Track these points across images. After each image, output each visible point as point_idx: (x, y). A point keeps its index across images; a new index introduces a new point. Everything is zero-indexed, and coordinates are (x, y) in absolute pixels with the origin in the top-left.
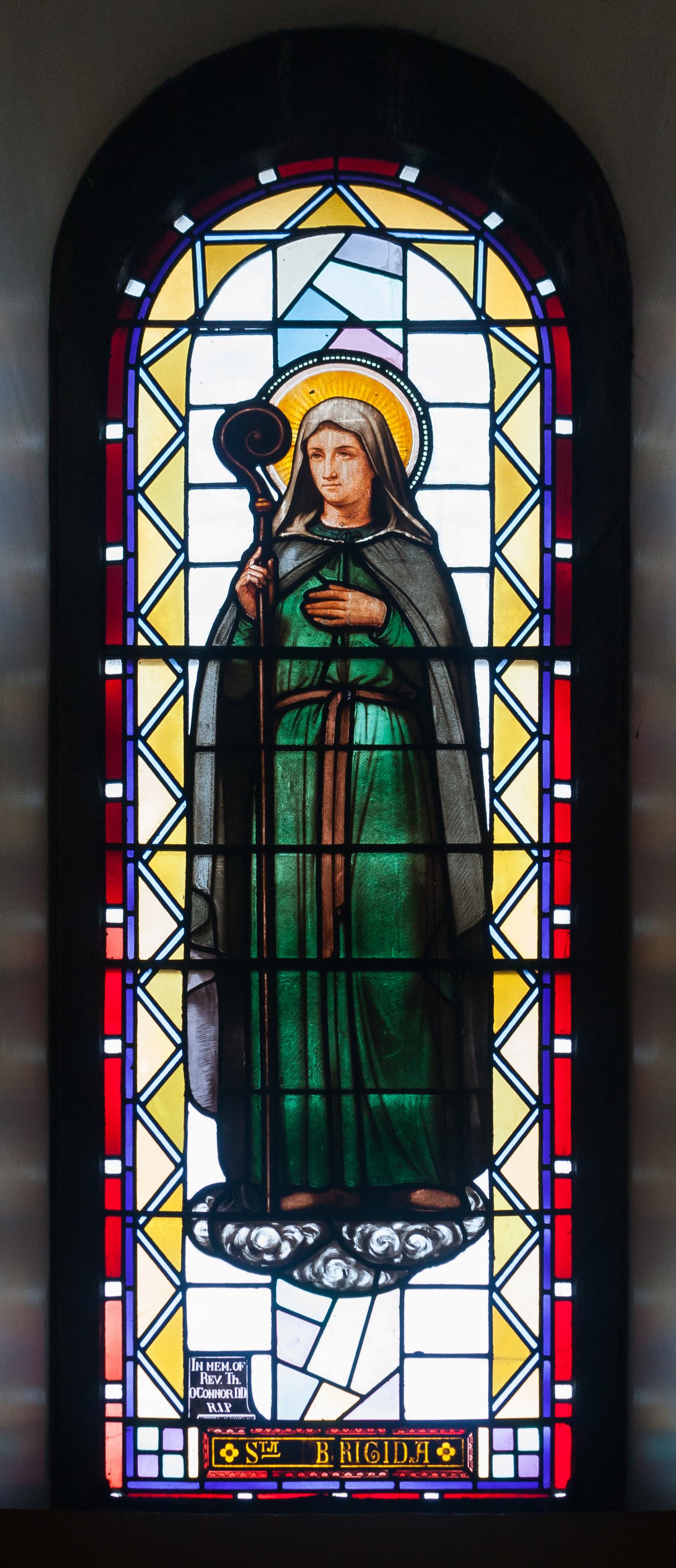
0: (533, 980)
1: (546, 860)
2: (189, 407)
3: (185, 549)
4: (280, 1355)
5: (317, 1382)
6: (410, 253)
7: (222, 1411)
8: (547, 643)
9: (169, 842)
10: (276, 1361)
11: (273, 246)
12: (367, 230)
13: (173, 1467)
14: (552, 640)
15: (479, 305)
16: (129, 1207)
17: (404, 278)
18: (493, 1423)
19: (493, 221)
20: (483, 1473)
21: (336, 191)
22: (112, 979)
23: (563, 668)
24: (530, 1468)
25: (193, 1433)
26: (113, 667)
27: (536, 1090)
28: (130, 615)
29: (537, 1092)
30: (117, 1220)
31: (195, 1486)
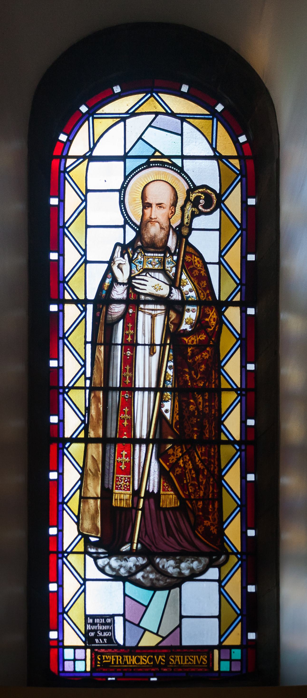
0: (238, 448)
1: (243, 450)
2: (88, 191)
3: (85, 255)
4: (127, 617)
5: (143, 630)
6: (185, 124)
7: (102, 642)
8: (244, 300)
9: (77, 385)
10: (125, 620)
11: (124, 120)
12: (166, 114)
13: (80, 667)
14: (246, 385)
15: (214, 146)
16: (60, 550)
17: (181, 135)
18: (220, 647)
19: (220, 108)
20: (216, 668)
21: (152, 96)
22: (52, 558)
23: (251, 311)
24: (237, 668)
25: (89, 651)
26: (54, 308)
27: (239, 168)
28: (61, 282)
29: (239, 332)
30: (55, 555)
31: (89, 675)
